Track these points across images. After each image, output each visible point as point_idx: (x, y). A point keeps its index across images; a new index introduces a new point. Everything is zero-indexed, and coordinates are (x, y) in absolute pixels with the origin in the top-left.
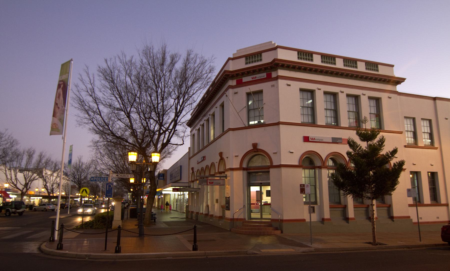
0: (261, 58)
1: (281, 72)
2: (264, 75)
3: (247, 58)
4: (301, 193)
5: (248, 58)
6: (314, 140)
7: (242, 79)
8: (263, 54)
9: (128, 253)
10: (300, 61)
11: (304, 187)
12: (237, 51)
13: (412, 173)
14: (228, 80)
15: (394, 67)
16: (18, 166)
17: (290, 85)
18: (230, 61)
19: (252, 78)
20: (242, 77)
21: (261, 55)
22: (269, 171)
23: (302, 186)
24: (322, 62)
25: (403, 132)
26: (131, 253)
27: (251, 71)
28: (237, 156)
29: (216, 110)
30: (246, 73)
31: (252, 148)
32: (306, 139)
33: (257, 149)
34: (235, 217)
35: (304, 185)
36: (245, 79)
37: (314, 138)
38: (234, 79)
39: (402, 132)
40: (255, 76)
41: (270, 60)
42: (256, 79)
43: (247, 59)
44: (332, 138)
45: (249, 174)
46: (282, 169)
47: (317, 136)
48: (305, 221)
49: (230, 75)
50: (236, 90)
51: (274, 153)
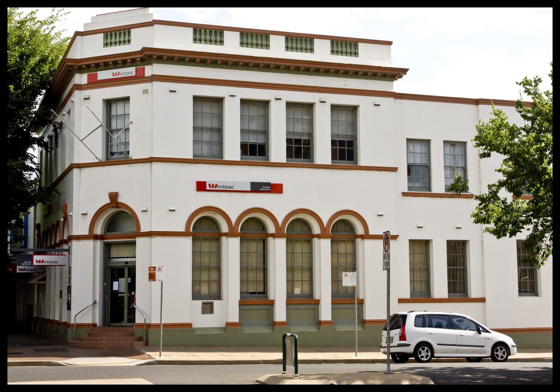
0: (129, 38)
2: (131, 71)
3: (107, 35)
6: (216, 187)
7: (96, 75)
11: (154, 272)
13: (412, 242)
14: (75, 75)
16: (538, 229)
18: (78, 38)
19: (113, 74)
20: (97, 71)
22: (136, 241)
23: (151, 269)
27: (230, 62)
28: (86, 214)
30: (120, 62)
31: (109, 201)
32: (201, 186)
35: (154, 268)
36: (103, 75)
37: (216, 185)
38: (85, 73)
39: (397, 168)
42: (119, 76)
43: (106, 37)
45: (107, 247)
48: (192, 327)
49: (75, 67)
51: (143, 211)
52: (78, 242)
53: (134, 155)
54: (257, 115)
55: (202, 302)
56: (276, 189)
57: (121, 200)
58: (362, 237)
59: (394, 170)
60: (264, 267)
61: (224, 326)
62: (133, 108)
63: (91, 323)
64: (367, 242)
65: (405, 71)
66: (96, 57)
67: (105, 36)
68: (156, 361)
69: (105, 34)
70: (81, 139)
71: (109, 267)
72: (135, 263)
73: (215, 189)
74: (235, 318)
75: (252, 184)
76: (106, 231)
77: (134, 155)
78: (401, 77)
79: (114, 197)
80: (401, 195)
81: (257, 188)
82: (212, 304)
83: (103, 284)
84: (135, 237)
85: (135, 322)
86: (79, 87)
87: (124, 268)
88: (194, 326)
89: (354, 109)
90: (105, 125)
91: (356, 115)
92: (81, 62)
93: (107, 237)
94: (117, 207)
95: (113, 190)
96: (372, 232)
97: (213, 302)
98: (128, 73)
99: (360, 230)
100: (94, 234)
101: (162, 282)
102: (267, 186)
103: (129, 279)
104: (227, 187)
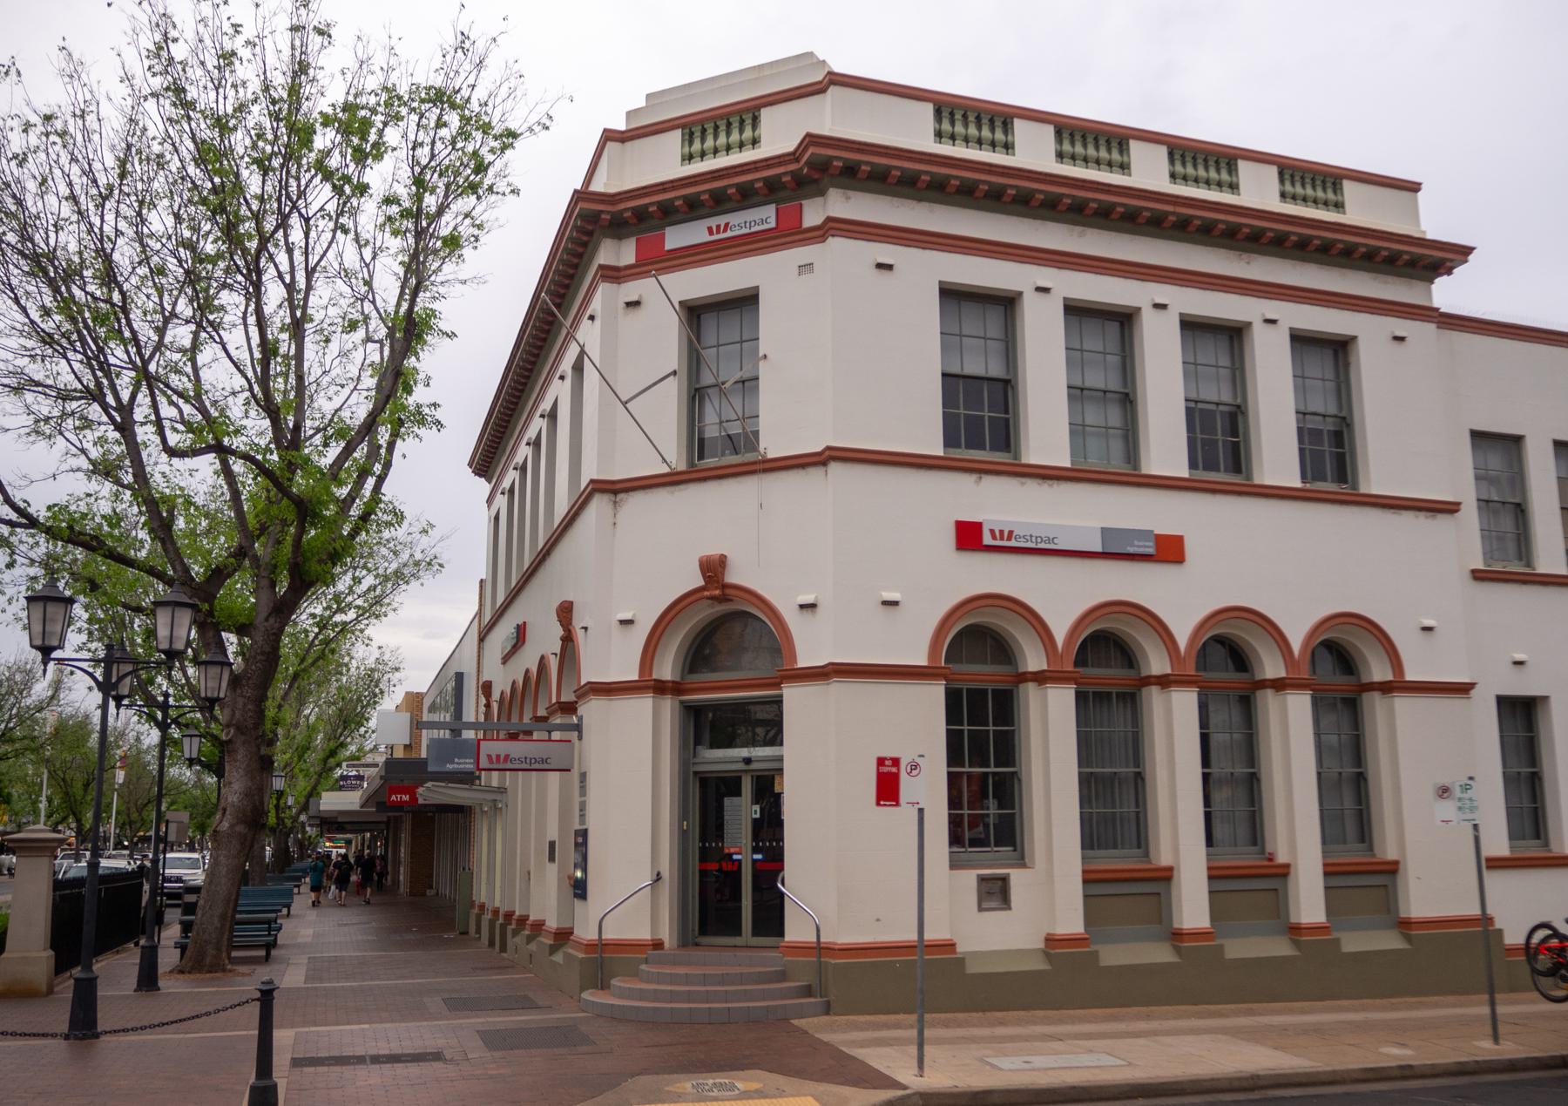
1: (840, 204)
2: (764, 217)
3: (691, 134)
4: (878, 804)
5: (697, 130)
6: (1009, 539)
8: (765, 114)
9: (1336, 1095)
10: (946, 149)
12: (649, 96)
13: (1501, 700)
15: (1419, 194)
17: (889, 267)
21: (755, 121)
22: (781, 696)
24: (1060, 156)
25: (1462, 506)
26: (1283, 1098)
29: (559, 391)
31: (700, 582)
32: (969, 536)
33: (725, 586)
34: (609, 935)
36: (677, 237)
37: (1011, 532)
38: (628, 236)
39: (1459, 504)
40: (721, 220)
41: (788, 145)
42: (729, 234)
43: (689, 138)
44: (1104, 531)
46: (1049, 690)
47: (1022, 519)
48: (954, 952)
50: (632, 290)
52: (607, 702)
53: (773, 445)
54: (1105, 348)
55: (978, 876)
56: (1169, 550)
57: (734, 577)
58: (1386, 688)
59: (1451, 508)
60: (1206, 770)
61: (1041, 945)
62: (771, 321)
63: (647, 940)
64: (1403, 705)
65: (1464, 252)
66: (662, 184)
67: (687, 137)
68: (914, 1094)
69: (687, 131)
70: (624, 399)
71: (696, 773)
72: (782, 760)
73: (1008, 547)
74: (1072, 922)
75: (1105, 532)
76: (686, 672)
77: (773, 445)
78: (1449, 272)
79: (713, 569)
80: (1468, 575)
81: (1116, 550)
82: (1004, 880)
83: (680, 826)
84: (777, 685)
85: (781, 933)
86: (614, 275)
87: (740, 778)
88: (959, 949)
89: (1340, 348)
90: (684, 374)
91: (1347, 365)
92: (621, 201)
93: (689, 686)
94: (723, 599)
95: (713, 551)
96: (1410, 676)
97: (1009, 874)
98: (753, 224)
99: (1379, 672)
100: (654, 677)
101: (921, 811)
102: (1146, 541)
103: (757, 808)
104: (533, 761)
